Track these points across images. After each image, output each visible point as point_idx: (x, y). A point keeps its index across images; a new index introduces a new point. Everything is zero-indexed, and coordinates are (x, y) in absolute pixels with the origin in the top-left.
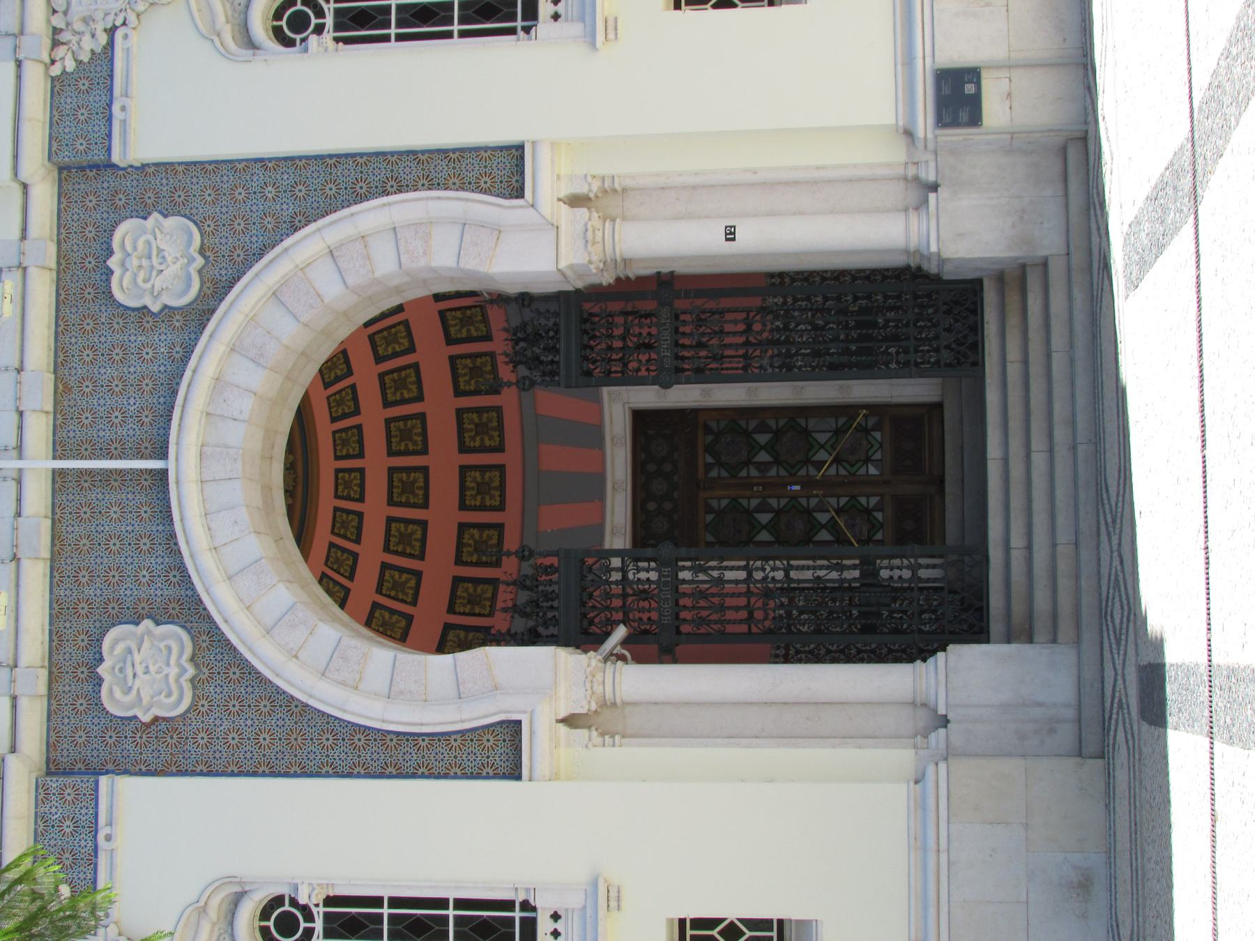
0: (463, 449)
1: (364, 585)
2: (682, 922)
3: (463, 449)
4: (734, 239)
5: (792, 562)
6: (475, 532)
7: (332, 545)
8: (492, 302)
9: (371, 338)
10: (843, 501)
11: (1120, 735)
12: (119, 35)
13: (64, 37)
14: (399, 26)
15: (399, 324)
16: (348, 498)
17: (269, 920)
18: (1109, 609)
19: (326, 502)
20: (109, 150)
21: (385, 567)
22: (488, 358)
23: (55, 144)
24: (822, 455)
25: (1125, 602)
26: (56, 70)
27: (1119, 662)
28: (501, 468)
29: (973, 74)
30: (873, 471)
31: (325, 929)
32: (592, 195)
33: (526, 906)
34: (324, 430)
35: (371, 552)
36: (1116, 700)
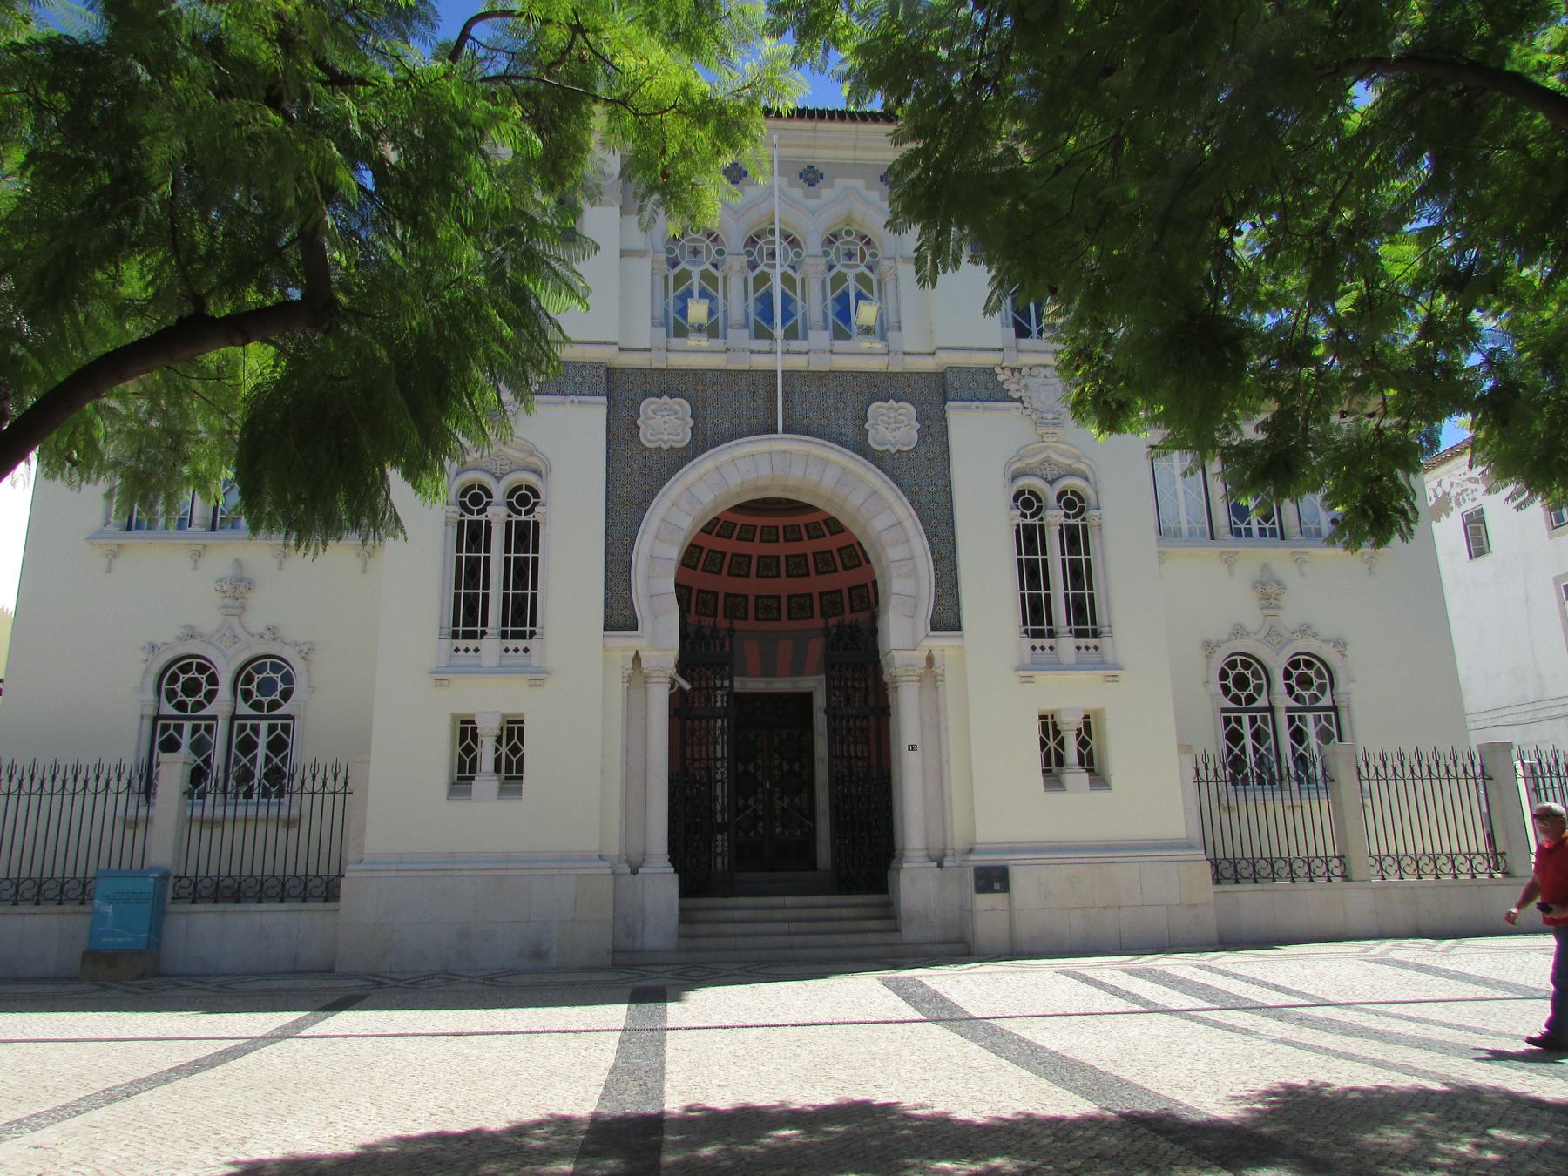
10: (761, 813)
11: (625, 976)
19: (759, 521)
24: (787, 800)
26: (998, 370)
27: (667, 974)
29: (1006, 888)
33: (532, 634)
34: (801, 520)
35: (731, 546)
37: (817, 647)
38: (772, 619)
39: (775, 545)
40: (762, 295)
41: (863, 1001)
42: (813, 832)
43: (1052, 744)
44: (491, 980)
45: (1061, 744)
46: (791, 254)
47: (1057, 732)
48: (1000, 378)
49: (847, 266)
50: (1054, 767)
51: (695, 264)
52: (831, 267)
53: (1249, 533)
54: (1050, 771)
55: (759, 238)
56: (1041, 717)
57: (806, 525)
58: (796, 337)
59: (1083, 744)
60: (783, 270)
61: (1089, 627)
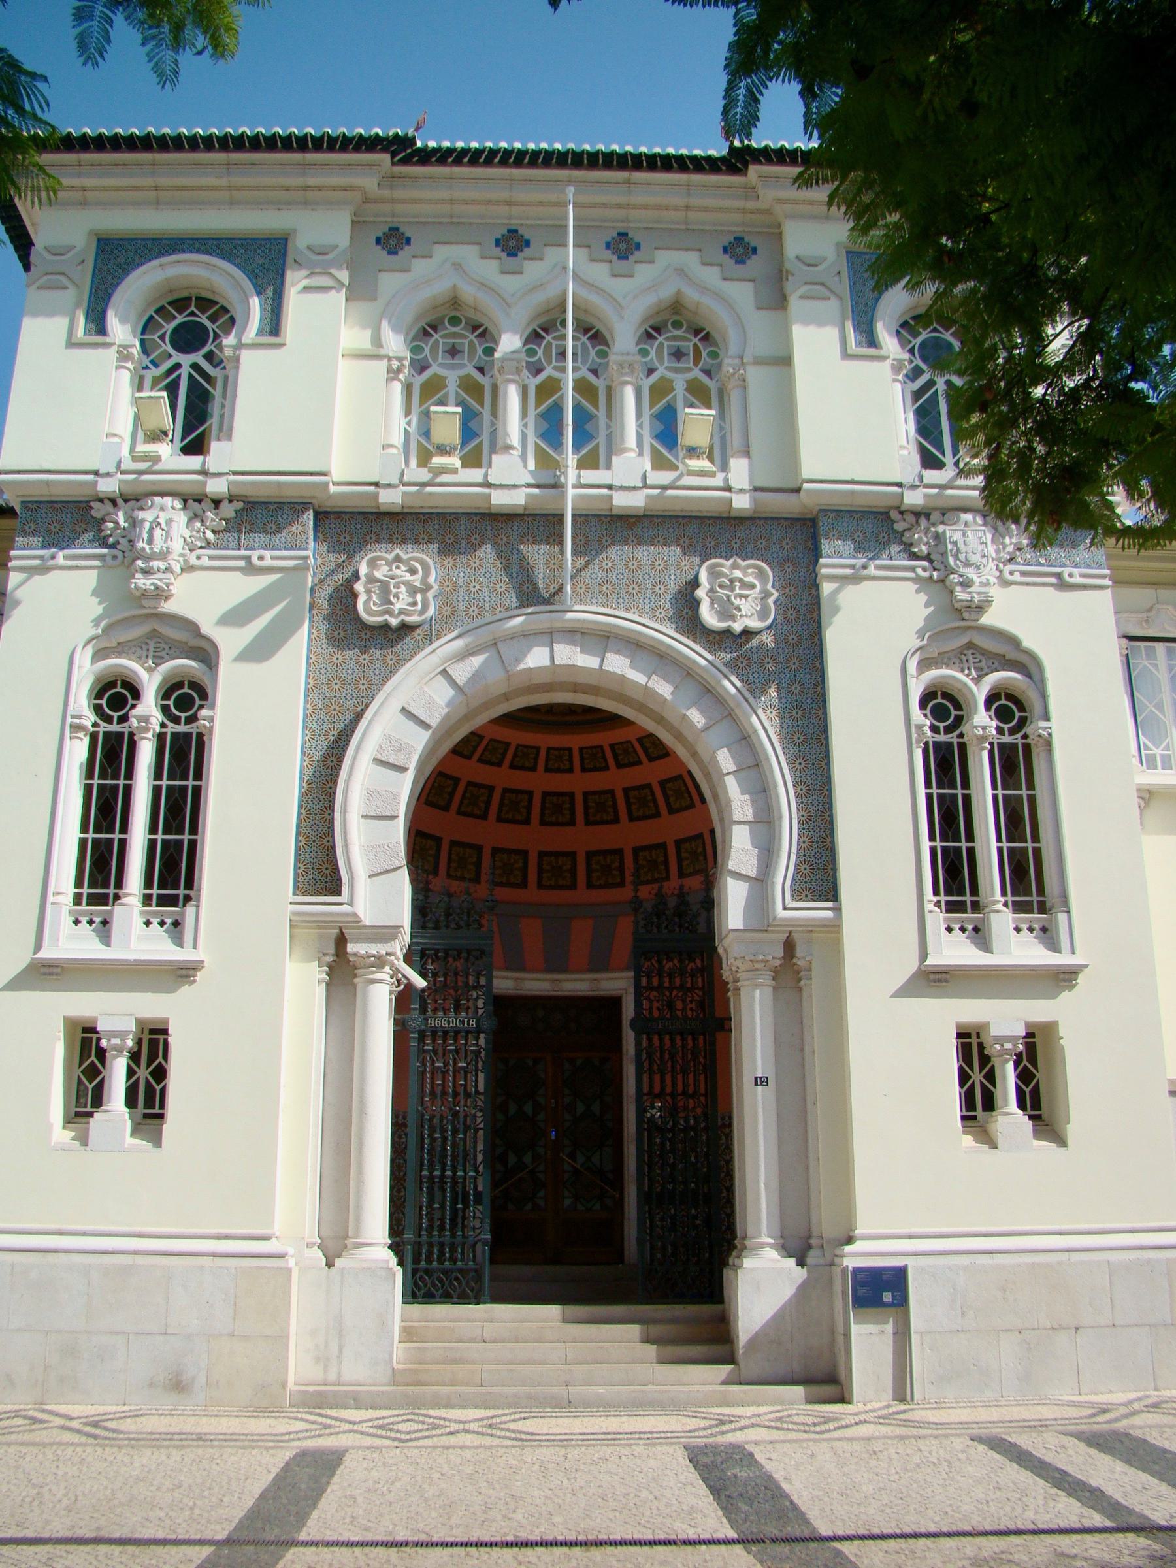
0: (590, 855)
1: (473, 771)
2: (165, 1032)
3: (590, 855)
4: (756, 1084)
5: (481, 1133)
6: (520, 864)
7: (508, 745)
8: (707, 876)
9: (680, 777)
10: (542, 1176)
11: (301, 1425)
12: (925, 563)
13: (923, 522)
14: (939, 795)
15: (691, 799)
16: (547, 760)
17: (189, 688)
18: (416, 1418)
20: (829, 557)
21: (491, 789)
22: (664, 875)
23: (833, 515)
24: (581, 1159)
25: (413, 1436)
26: (894, 515)
28: (573, 886)
30: (567, 1202)
31: (178, 733)
32: (795, 960)
33: (188, 899)
35: (502, 778)
36: (333, 1422)
37: (625, 930)
38: (561, 887)
39: (566, 776)
40: (549, 410)
41: (644, 1494)
42: (620, 1204)
43: (977, 1077)
44: (96, 1425)
45: (991, 1076)
46: (593, 353)
47: (985, 1059)
48: (899, 526)
49: (676, 370)
50: (979, 1112)
51: (452, 367)
52: (651, 371)
53: (140, 389)
54: (974, 1118)
55: (546, 330)
56: (960, 1036)
57: (612, 746)
58: (596, 467)
59: (1024, 1076)
60: (579, 374)
61: (1035, 898)
